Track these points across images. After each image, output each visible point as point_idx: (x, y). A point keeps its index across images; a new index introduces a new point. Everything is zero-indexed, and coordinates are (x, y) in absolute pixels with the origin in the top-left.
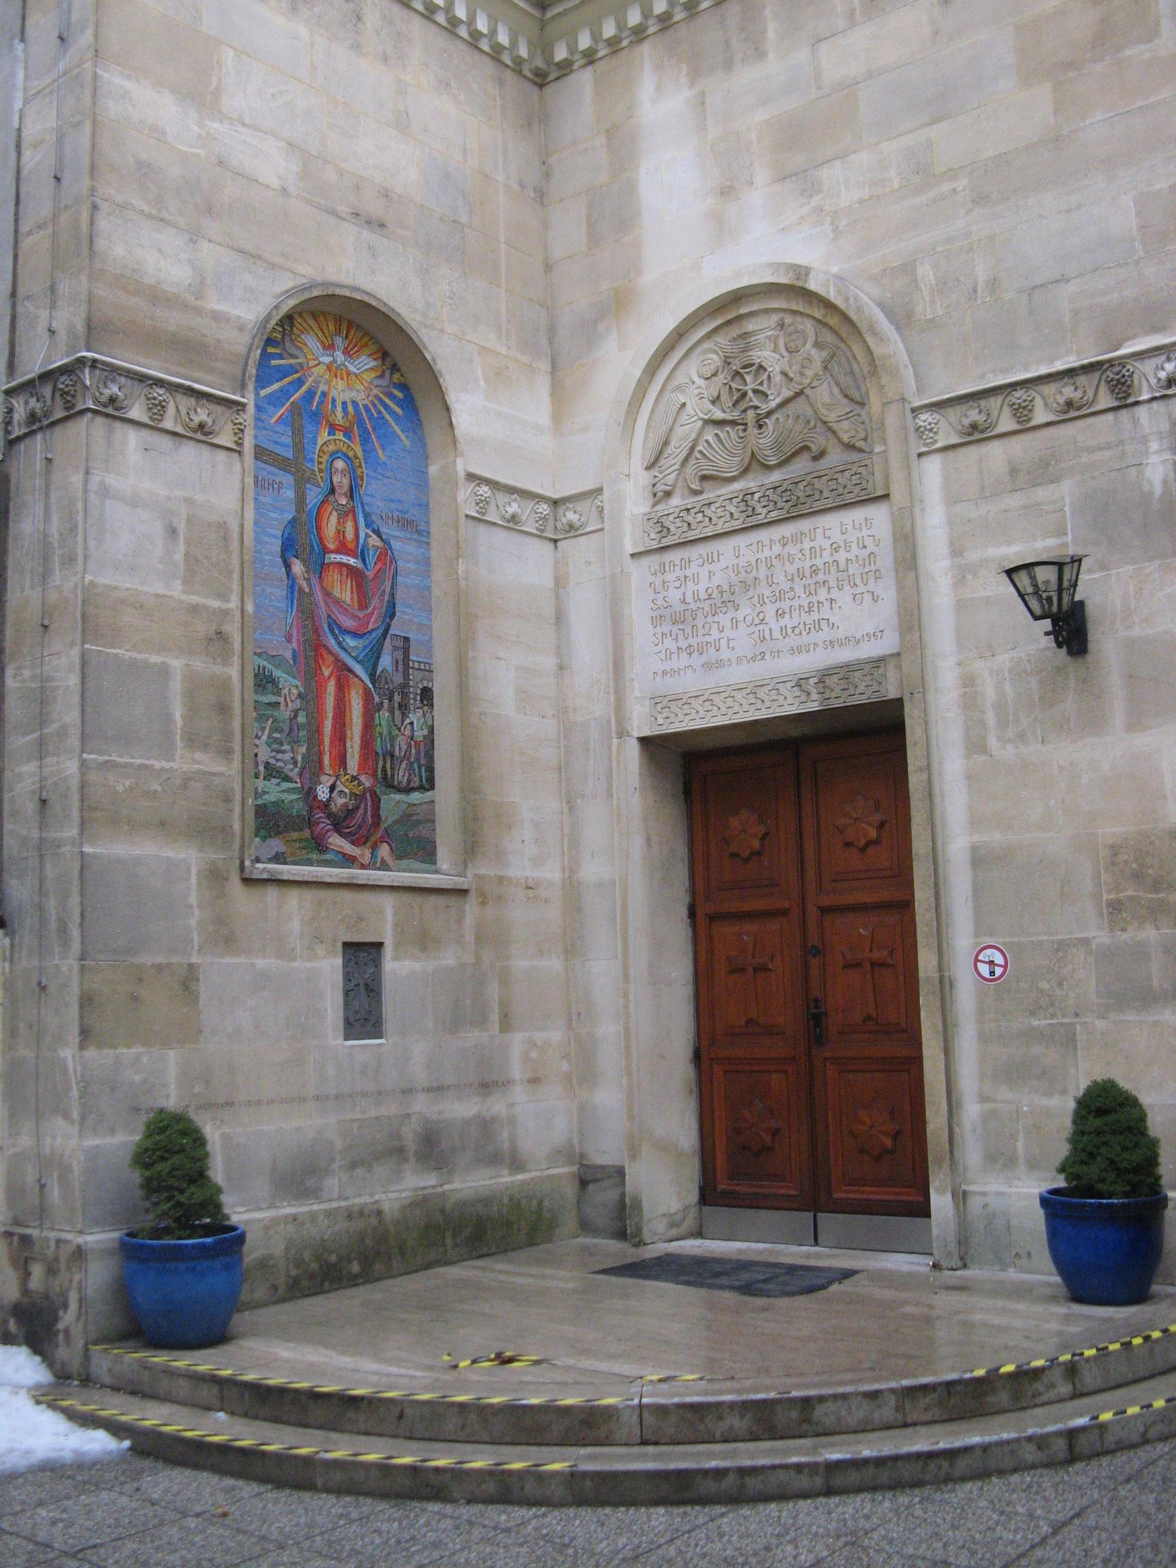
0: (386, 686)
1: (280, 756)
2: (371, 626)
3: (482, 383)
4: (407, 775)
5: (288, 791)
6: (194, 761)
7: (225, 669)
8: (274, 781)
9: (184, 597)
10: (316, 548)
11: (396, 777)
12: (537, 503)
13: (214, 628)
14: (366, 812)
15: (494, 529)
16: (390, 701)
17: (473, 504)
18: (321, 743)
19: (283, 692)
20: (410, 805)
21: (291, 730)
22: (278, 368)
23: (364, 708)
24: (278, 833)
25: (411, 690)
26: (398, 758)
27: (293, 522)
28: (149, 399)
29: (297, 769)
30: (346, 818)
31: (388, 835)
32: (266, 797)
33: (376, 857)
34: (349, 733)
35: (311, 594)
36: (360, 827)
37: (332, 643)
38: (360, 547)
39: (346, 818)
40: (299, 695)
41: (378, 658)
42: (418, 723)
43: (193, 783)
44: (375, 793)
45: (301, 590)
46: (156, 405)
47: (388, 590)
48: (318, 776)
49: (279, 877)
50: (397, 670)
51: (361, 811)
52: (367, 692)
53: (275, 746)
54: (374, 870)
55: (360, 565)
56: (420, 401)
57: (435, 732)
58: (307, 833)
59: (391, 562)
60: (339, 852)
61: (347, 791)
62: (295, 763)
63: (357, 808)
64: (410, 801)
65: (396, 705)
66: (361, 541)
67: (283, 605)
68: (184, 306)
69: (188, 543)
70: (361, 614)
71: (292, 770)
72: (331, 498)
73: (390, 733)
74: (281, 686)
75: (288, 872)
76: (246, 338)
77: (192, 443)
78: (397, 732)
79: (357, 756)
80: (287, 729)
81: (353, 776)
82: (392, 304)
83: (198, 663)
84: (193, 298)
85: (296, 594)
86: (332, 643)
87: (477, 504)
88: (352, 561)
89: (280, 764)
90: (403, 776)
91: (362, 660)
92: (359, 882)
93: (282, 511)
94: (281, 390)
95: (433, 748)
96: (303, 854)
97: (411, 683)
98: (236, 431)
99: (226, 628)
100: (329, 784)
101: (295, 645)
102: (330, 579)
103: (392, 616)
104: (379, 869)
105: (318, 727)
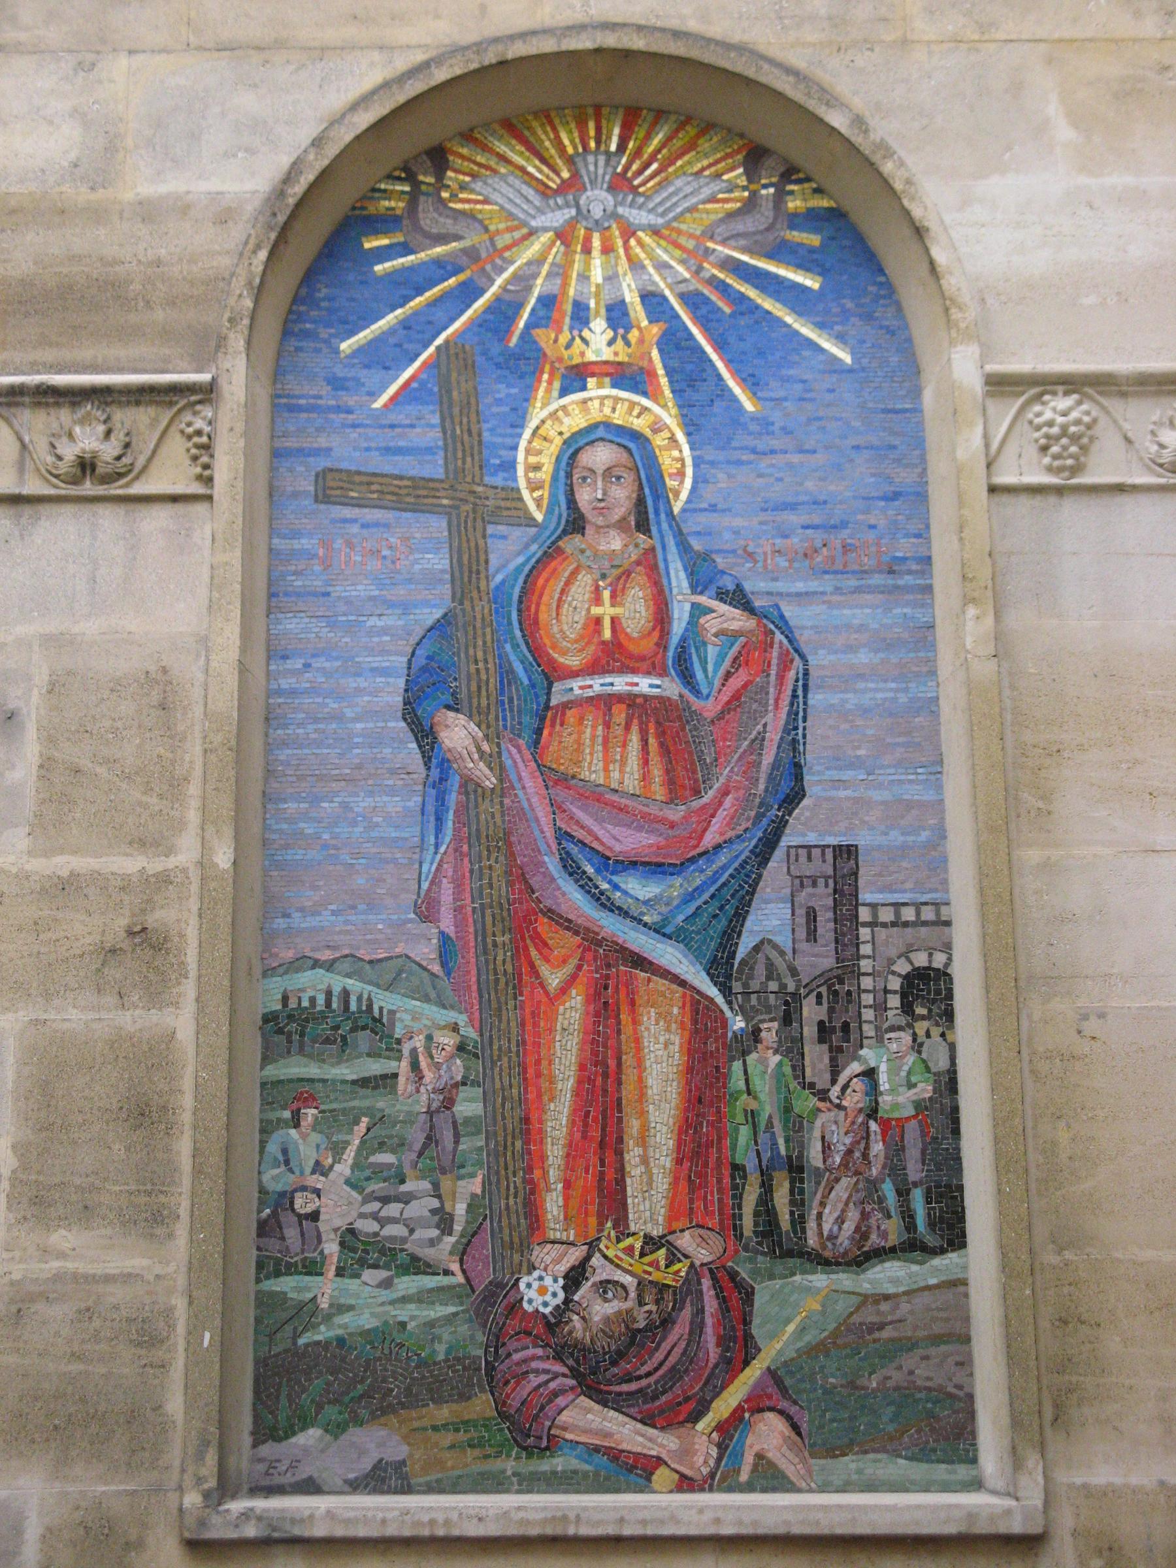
0: (773, 986)
1: (393, 1209)
2: (709, 839)
3: (1065, 133)
4: (853, 1215)
5: (422, 1298)
6: (45, 1252)
7: (154, 1016)
8: (370, 1275)
9: (38, 865)
10: (519, 668)
11: (811, 1225)
12: (1038, 398)
13: (123, 922)
14: (697, 1327)
15: (1127, 502)
16: (787, 1020)
17: (1032, 452)
18: (534, 1160)
19: (406, 1049)
20: (866, 1300)
21: (431, 1139)
22: (392, 278)
23: (690, 1052)
24: (383, 1411)
25: (867, 982)
26: (818, 1173)
27: (441, 627)
28: (189, 437)
29: (450, 1240)
30: (621, 1355)
31: (784, 1391)
32: (346, 1318)
33: (739, 1455)
34: (633, 1126)
35: (504, 788)
36: (675, 1374)
37: (574, 900)
38: (674, 640)
39: (621, 1355)
40: (461, 1048)
41: (740, 915)
42: (893, 1071)
43: (40, 1306)
44: (733, 1275)
45: (469, 785)
46: (1057, 438)
47: (774, 736)
48: (524, 1247)
49: (297, 1531)
50: (812, 935)
51: (680, 1329)
52: (699, 1007)
53: (374, 1187)
54: (730, 1490)
55: (671, 688)
56: (877, 241)
57: (962, 1086)
58: (482, 1404)
59: (785, 665)
60: (597, 1449)
61: (627, 1280)
62: (445, 1222)
63: (667, 1322)
64: (866, 1287)
65: (810, 1031)
66: (678, 628)
67: (412, 833)
68: (62, 213)
69: (49, 739)
70: (676, 813)
71: (432, 1243)
72: (572, 544)
73: (787, 1109)
74: (399, 1032)
75: (330, 1515)
76: (238, 232)
77: (68, 509)
78: (813, 1101)
79: (662, 1184)
80: (417, 1137)
81: (648, 1239)
82: (717, 30)
83: (74, 1014)
84: (84, 189)
85: (453, 798)
86: (574, 900)
87: (1044, 449)
88: (644, 684)
89: (391, 1230)
90: (840, 1220)
91: (680, 930)
92: (584, 1531)
93: (406, 607)
94: (405, 325)
95: (956, 1132)
96: (474, 1465)
97: (865, 965)
98: (194, 451)
99: (159, 917)
100: (563, 1268)
101: (447, 923)
102: (569, 740)
103: (794, 797)
104: (749, 1488)
105: (526, 1120)
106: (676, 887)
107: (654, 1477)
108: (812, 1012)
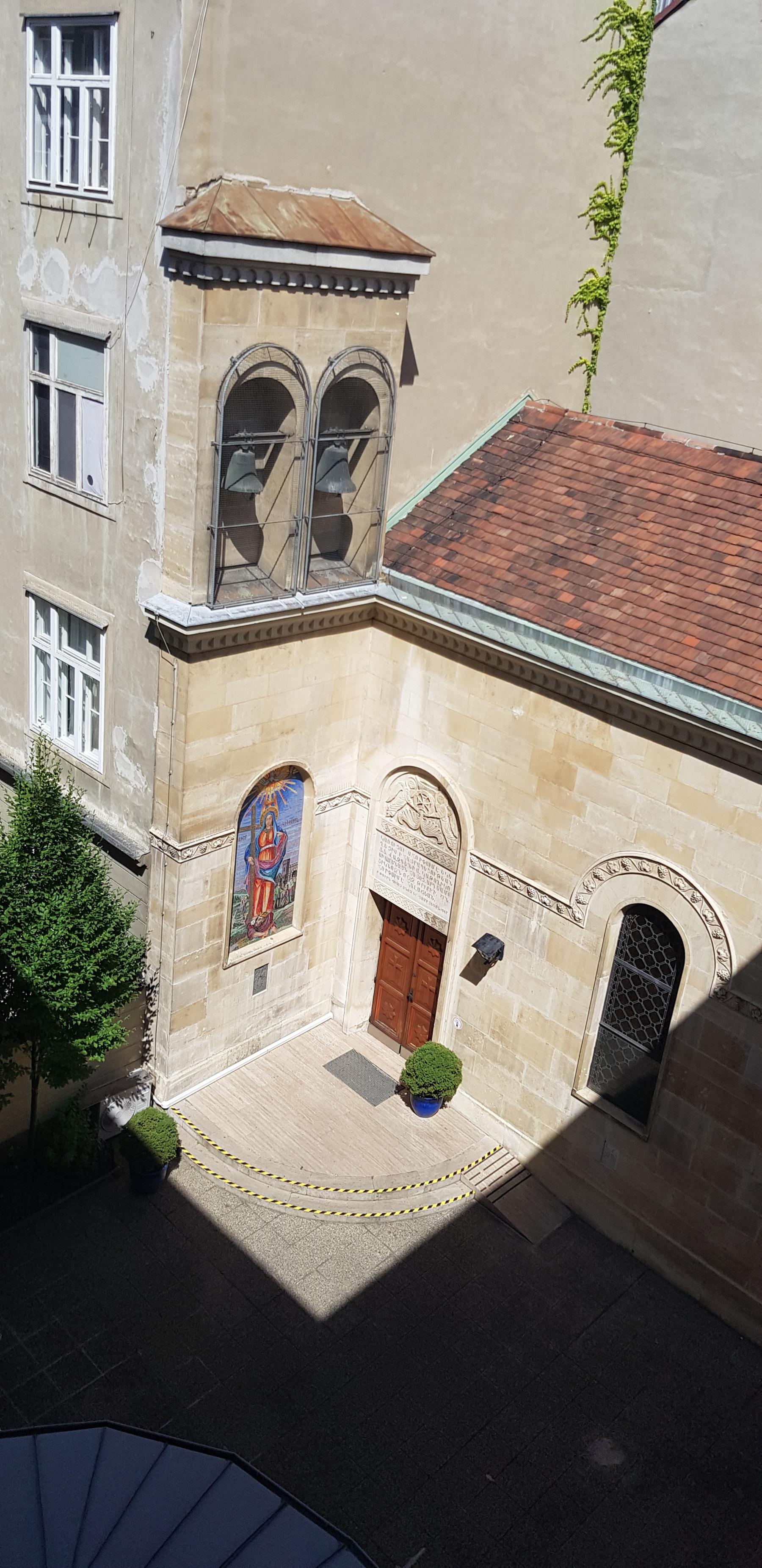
37: (261, 876)
86: (261, 876)
106: (271, 870)
107: (335, 550)
108: (283, 880)
